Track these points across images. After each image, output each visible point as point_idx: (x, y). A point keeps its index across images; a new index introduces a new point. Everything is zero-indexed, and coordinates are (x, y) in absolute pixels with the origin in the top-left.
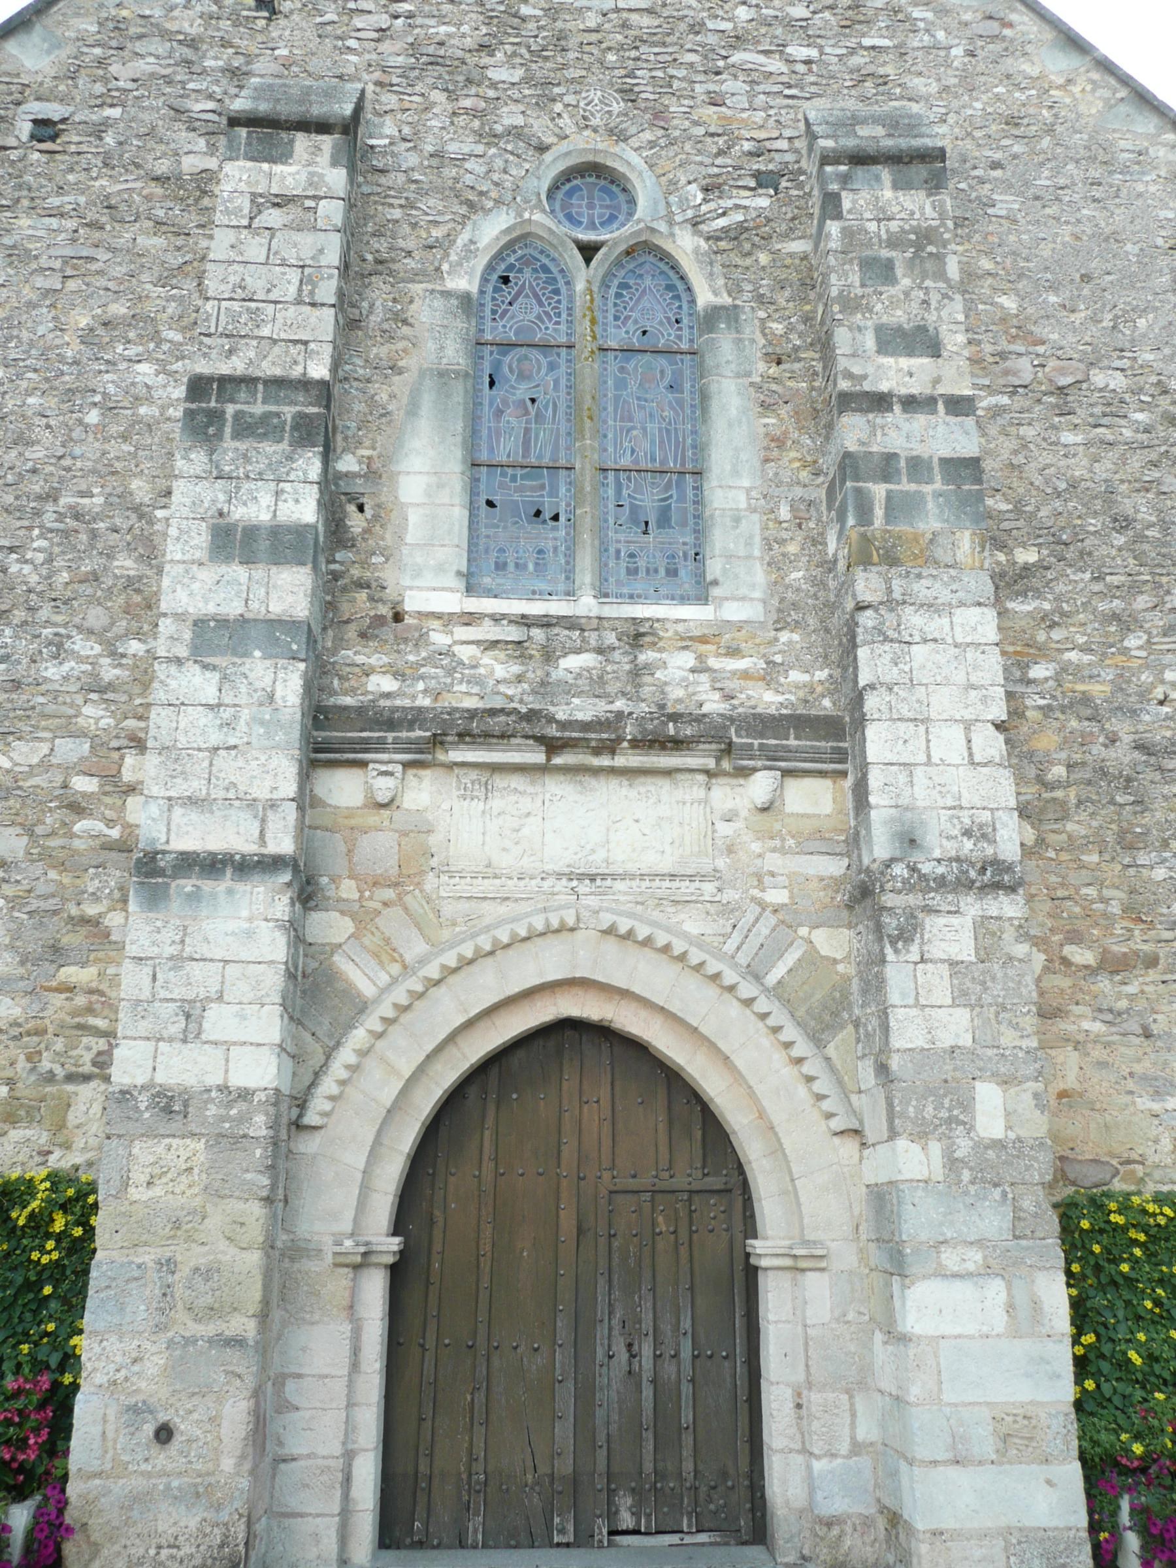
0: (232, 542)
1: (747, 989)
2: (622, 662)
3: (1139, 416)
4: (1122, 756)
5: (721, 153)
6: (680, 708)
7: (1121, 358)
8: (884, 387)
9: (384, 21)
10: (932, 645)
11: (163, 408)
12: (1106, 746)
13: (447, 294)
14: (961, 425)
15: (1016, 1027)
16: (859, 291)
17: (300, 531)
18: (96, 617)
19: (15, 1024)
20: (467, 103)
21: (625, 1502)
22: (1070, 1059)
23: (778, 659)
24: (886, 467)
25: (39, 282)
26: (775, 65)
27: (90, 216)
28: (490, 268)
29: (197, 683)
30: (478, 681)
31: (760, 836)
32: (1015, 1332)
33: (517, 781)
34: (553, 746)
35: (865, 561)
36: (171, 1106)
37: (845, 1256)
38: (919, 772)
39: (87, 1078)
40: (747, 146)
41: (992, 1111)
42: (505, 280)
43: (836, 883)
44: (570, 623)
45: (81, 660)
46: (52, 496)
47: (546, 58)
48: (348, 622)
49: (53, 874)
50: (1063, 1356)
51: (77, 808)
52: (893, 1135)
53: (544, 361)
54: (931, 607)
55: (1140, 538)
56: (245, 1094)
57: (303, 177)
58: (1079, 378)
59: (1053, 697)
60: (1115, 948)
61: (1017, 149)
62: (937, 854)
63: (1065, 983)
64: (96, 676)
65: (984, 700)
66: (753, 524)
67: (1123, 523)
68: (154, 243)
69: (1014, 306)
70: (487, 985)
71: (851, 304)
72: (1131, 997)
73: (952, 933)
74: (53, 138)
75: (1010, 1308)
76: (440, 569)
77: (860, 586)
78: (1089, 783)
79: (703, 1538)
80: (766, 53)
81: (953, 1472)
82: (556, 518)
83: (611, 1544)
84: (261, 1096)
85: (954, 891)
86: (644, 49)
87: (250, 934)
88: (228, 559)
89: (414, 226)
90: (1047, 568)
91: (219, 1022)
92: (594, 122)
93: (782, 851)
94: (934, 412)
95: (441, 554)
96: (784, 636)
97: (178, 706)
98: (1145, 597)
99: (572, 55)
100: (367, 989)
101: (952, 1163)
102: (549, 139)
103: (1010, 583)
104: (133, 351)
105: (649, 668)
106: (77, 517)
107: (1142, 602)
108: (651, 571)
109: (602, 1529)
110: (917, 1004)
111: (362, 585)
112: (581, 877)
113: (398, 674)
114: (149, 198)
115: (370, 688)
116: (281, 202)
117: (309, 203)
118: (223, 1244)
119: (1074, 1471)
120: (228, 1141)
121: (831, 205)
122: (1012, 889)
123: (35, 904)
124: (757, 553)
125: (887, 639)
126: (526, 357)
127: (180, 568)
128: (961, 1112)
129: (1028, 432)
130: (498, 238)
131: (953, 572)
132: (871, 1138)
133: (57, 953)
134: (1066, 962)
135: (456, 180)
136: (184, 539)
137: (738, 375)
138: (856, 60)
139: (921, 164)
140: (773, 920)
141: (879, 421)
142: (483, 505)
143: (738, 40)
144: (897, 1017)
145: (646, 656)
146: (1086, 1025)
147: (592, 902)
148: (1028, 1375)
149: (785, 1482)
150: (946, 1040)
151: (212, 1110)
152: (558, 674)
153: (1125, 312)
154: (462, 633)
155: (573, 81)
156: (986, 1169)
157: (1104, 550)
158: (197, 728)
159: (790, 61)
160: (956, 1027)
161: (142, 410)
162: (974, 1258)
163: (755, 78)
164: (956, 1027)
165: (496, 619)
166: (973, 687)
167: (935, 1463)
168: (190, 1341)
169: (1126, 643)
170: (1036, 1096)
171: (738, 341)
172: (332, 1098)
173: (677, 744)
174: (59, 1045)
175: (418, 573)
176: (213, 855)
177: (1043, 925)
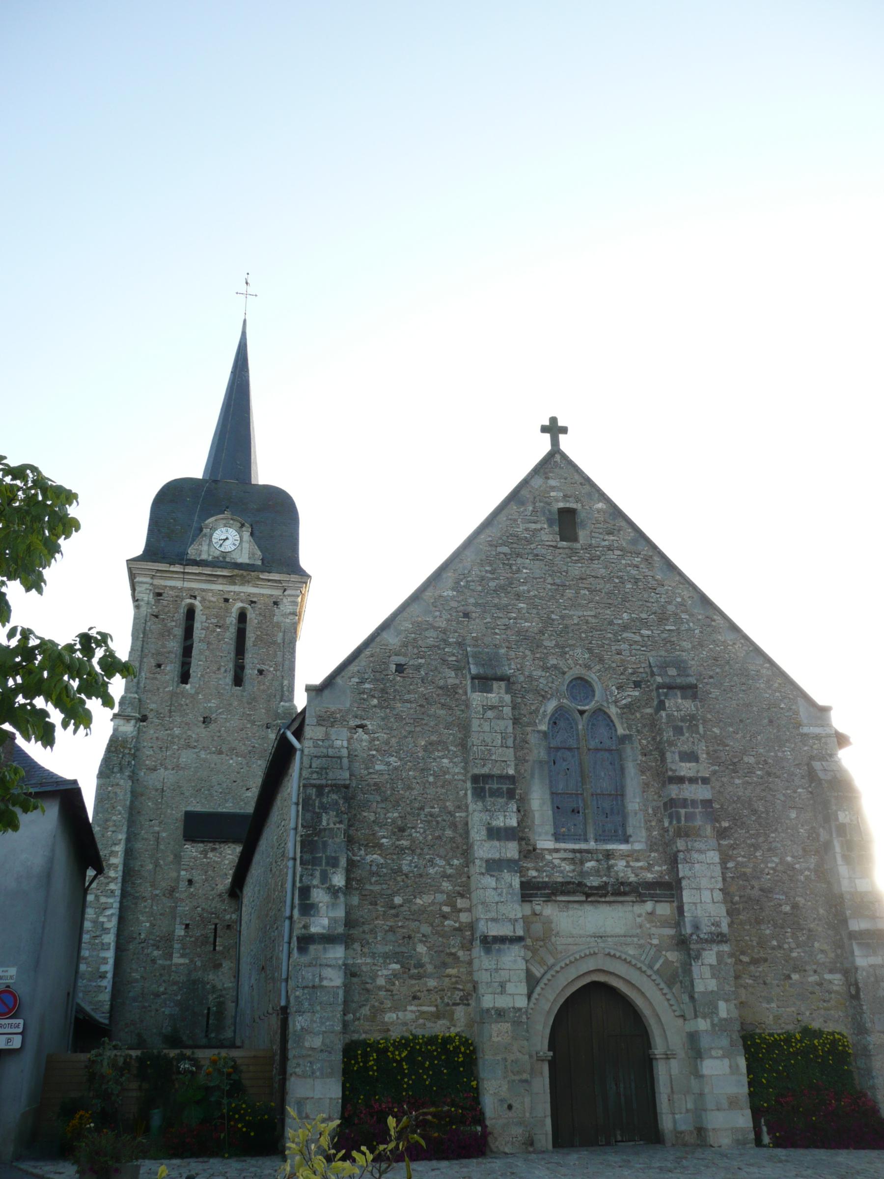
0: (494, 833)
1: (649, 972)
3: (759, 773)
4: (756, 893)
5: (622, 674)
6: (623, 880)
8: (682, 774)
9: (506, 621)
11: (453, 776)
13: (539, 732)
15: (729, 984)
16: (673, 738)
17: (513, 829)
18: (442, 852)
19: (435, 988)
20: (538, 656)
22: (742, 991)
24: (684, 803)
25: (407, 728)
26: (637, 638)
27: (420, 702)
28: (550, 719)
30: (562, 872)
31: (651, 922)
33: (576, 906)
34: (588, 895)
35: (680, 836)
36: (501, 1014)
37: (681, 1054)
38: (699, 906)
39: (458, 1004)
40: (630, 671)
41: (724, 1010)
42: (555, 723)
43: (672, 937)
44: (588, 851)
45: (440, 867)
46: (422, 808)
49: (440, 939)
50: (745, 1080)
51: (445, 917)
52: (696, 1017)
54: (700, 851)
55: (760, 817)
56: (520, 1009)
57: (497, 699)
61: (718, 670)
63: (741, 967)
64: (444, 872)
66: (640, 816)
67: (754, 811)
68: (442, 712)
70: (572, 973)
71: (671, 744)
72: (760, 972)
73: (710, 956)
74: (402, 672)
75: (730, 1067)
76: (546, 833)
77: (679, 844)
79: (642, 1142)
80: (634, 633)
81: (717, 1113)
86: (595, 633)
87: (515, 961)
88: (493, 839)
89: (525, 705)
91: (510, 988)
92: (580, 662)
93: (656, 927)
94: (698, 783)
96: (653, 855)
97: (485, 888)
99: (571, 635)
100: (538, 975)
102: (566, 670)
103: (722, 834)
104: (440, 754)
105: (612, 866)
106: (431, 816)
107: (761, 839)
112: (598, 937)
113: (537, 870)
114: (438, 695)
116: (492, 708)
118: (518, 1054)
119: (748, 1112)
121: (661, 706)
122: (726, 942)
123: (436, 949)
125: (687, 862)
127: (479, 843)
128: (715, 1010)
129: (725, 780)
132: (688, 1017)
133: (445, 965)
134: (741, 961)
135: (537, 686)
137: (633, 761)
138: (664, 635)
139: (690, 691)
142: (557, 809)
143: (625, 628)
144: (697, 982)
145: (612, 862)
146: (747, 981)
147: (602, 945)
149: (666, 1123)
150: (710, 989)
154: (555, 855)
155: (572, 645)
156: (722, 1027)
158: (491, 896)
159: (642, 636)
160: (712, 985)
161: (447, 777)
162: (720, 1052)
165: (565, 850)
168: (514, 1081)
171: (632, 748)
173: (625, 894)
174: (449, 994)
175: (540, 835)
176: (501, 936)
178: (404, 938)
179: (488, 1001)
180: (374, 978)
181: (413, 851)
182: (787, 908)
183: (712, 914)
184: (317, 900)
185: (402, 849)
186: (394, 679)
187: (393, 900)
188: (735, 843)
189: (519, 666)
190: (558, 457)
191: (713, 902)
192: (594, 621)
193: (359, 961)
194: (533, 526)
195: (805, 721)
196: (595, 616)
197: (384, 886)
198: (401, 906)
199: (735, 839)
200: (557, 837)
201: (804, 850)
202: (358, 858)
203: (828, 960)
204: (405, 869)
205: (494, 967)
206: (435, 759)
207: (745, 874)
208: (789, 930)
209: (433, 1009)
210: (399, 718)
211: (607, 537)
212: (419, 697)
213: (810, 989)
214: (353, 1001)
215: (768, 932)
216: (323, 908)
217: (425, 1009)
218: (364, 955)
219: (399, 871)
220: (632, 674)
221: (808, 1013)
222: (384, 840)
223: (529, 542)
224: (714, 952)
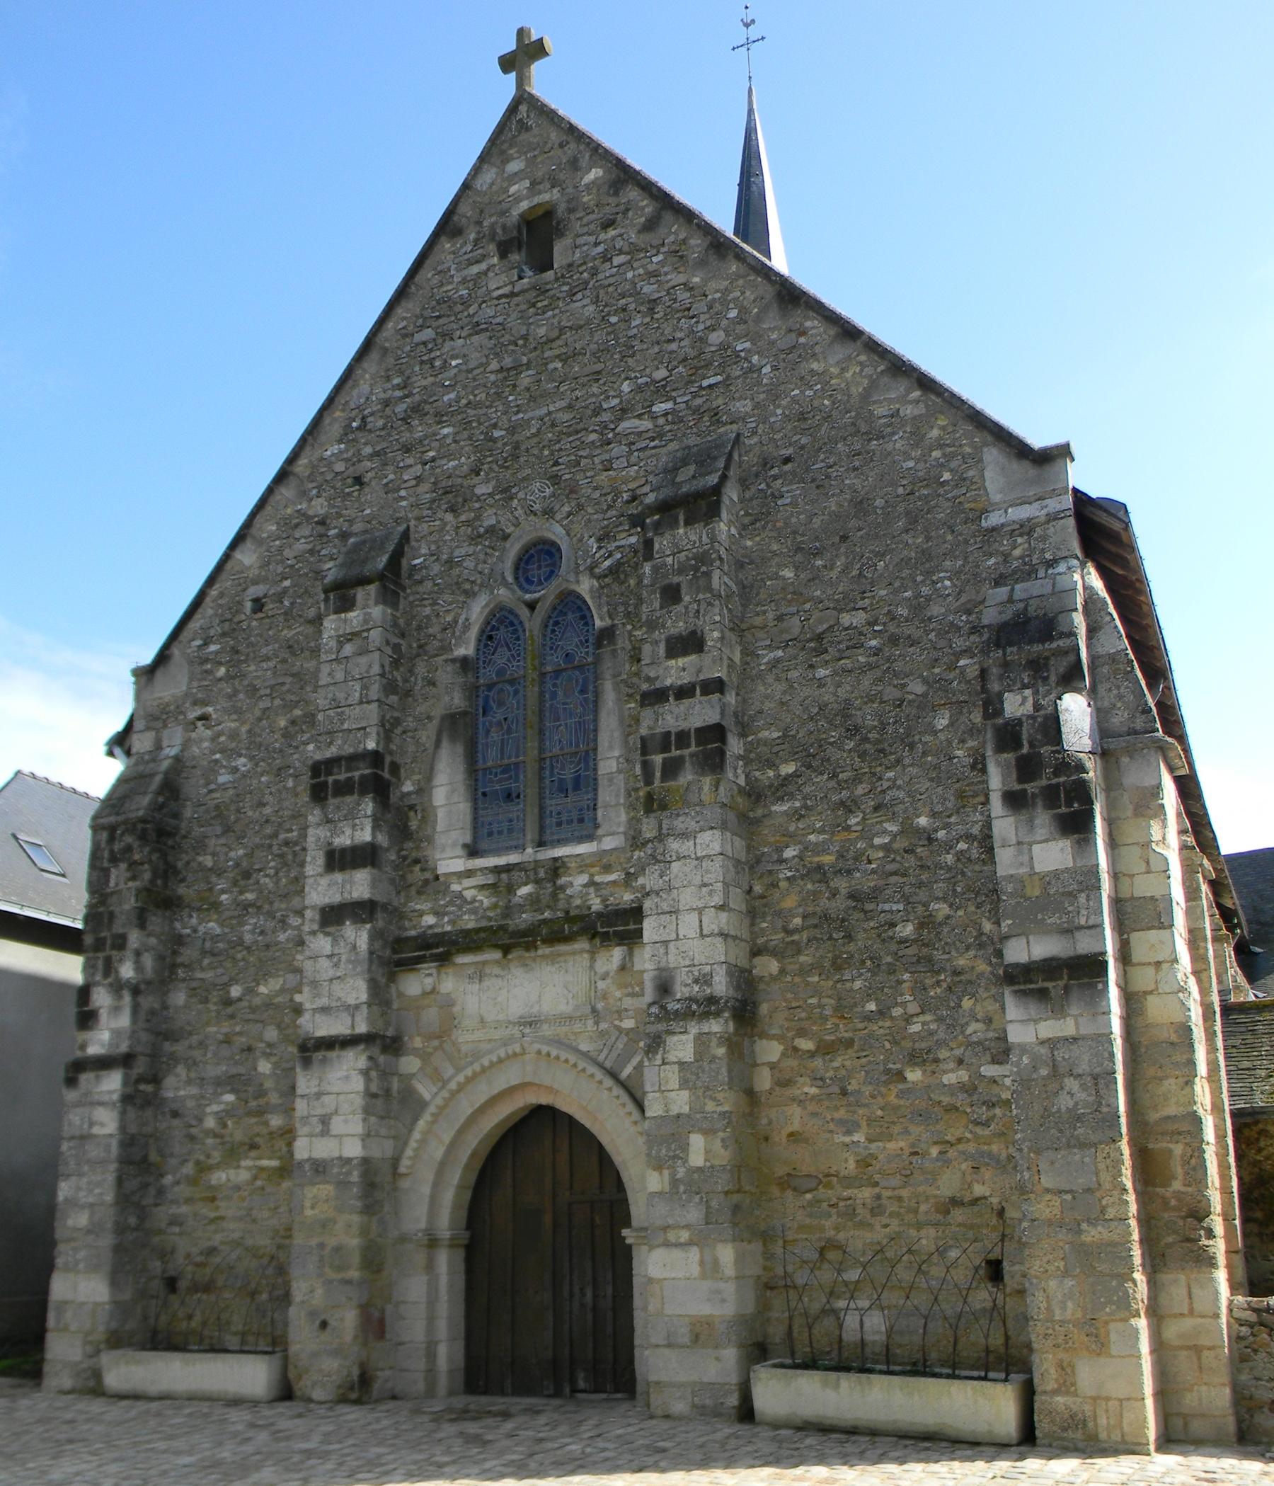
0: (339, 860)
2: (549, 888)
3: (874, 643)
4: (838, 905)
7: (863, 599)
8: (668, 682)
10: (683, 861)
12: (829, 899)
14: (709, 702)
15: (714, 1099)
21: (581, 1375)
23: (632, 870)
26: (646, 424)
28: (482, 632)
29: (322, 944)
31: (623, 986)
32: (703, 1276)
36: (319, 1168)
38: (671, 945)
42: (490, 638)
46: (276, 835)
47: (507, 468)
48: (411, 885)
53: (511, 690)
54: (684, 835)
55: (865, 740)
56: (349, 1160)
58: (832, 623)
59: (797, 870)
60: (827, 1038)
62: (678, 996)
65: (711, 893)
66: (620, 780)
67: (854, 731)
69: (792, 575)
70: (482, 1092)
71: (652, 625)
75: (702, 1263)
76: (454, 845)
78: (816, 926)
79: (619, 1396)
80: (639, 417)
81: (666, 1351)
82: (518, 797)
83: (571, 1397)
84: (355, 1162)
85: (684, 1019)
90: (799, 776)
91: (337, 1125)
95: (454, 835)
96: (637, 854)
97: (314, 958)
98: (864, 785)
100: (427, 1096)
101: (675, 1182)
107: (860, 790)
108: (570, 822)
109: (567, 1390)
110: (660, 1090)
111: (417, 861)
113: (436, 914)
115: (423, 924)
117: (365, 634)
120: (343, 1184)
124: (622, 801)
126: (502, 690)
129: (794, 674)
130: (481, 612)
131: (698, 808)
134: (796, 1049)
136: (314, 862)
140: (625, 1039)
141: (661, 710)
146: (806, 1090)
148: (709, 1300)
150: (675, 1110)
151: (335, 1170)
152: (516, 900)
153: (869, 559)
154: (468, 882)
157: (839, 754)
162: (685, 1235)
163: (631, 440)
164: (681, 1102)
166: (705, 885)
167: (657, 1346)
168: (331, 1282)
169: (849, 822)
170: (723, 1140)
172: (410, 1158)
175: (443, 850)
177: (781, 1027)
178: (243, 1050)
179: (303, 1149)
180: (200, 1120)
181: (259, 908)
182: (907, 930)
183: (699, 959)
184: (97, 1004)
185: (246, 906)
186: (249, 626)
187: (228, 992)
188: (806, 807)
189: (433, 547)
190: (523, 108)
191: (702, 936)
192: (566, 417)
193: (182, 1093)
194: (475, 269)
195: (996, 497)
196: (570, 407)
197: (220, 971)
198: (240, 999)
199: (805, 798)
200: (473, 851)
201: (960, 795)
202: (188, 931)
203: (991, 1035)
204: (248, 938)
205: (316, 1090)
206: (297, 748)
207: (819, 867)
208: (906, 976)
209: (274, 1163)
210: (253, 690)
211: (602, 236)
212: (281, 647)
213: (946, 1100)
214: (172, 1155)
215: (858, 984)
216: (104, 1015)
217: (265, 1163)
218: (189, 1082)
219: (241, 942)
220: (628, 502)
221: (934, 1151)
222: (224, 897)
223: (465, 303)
224: (691, 1037)
